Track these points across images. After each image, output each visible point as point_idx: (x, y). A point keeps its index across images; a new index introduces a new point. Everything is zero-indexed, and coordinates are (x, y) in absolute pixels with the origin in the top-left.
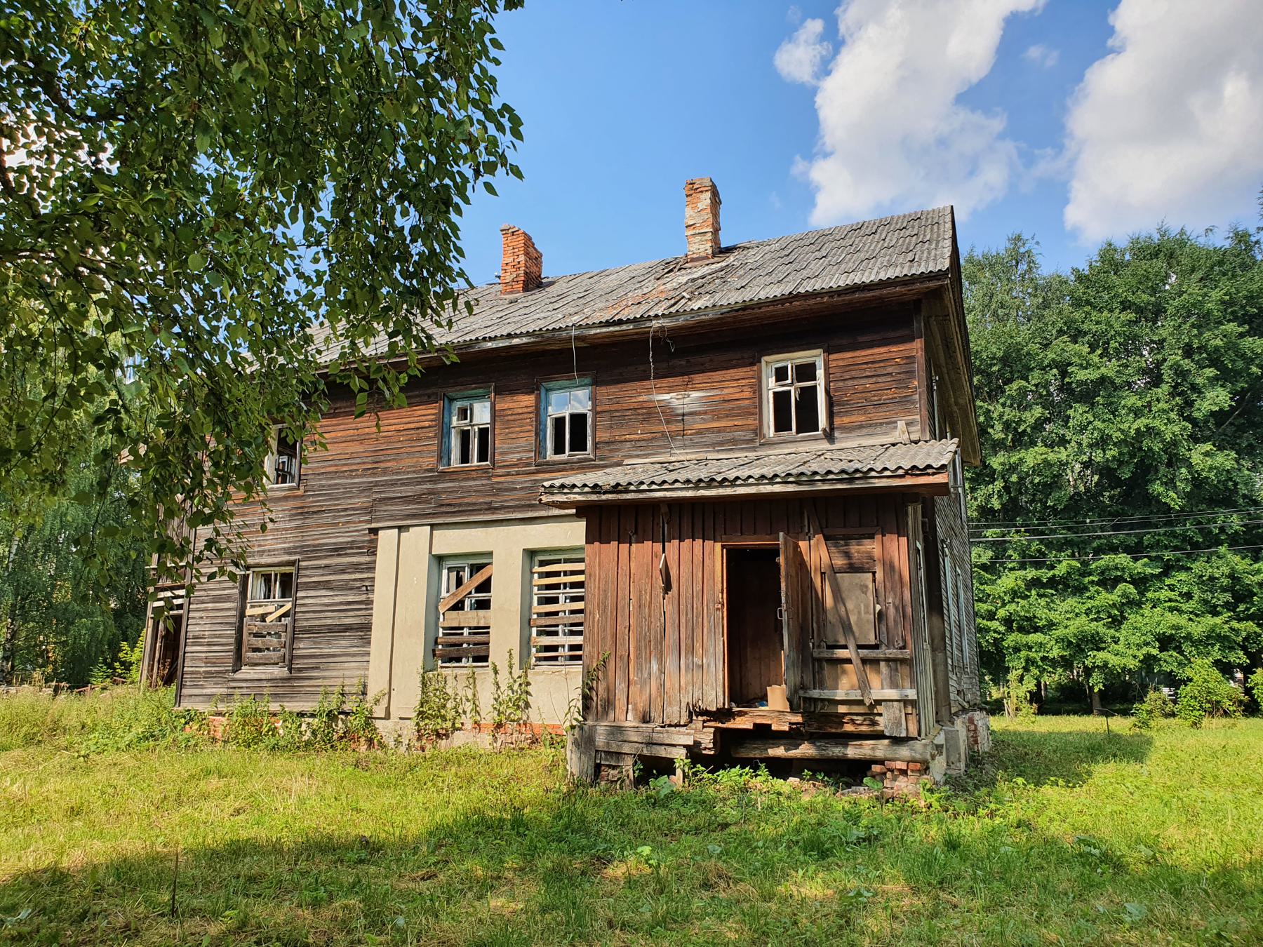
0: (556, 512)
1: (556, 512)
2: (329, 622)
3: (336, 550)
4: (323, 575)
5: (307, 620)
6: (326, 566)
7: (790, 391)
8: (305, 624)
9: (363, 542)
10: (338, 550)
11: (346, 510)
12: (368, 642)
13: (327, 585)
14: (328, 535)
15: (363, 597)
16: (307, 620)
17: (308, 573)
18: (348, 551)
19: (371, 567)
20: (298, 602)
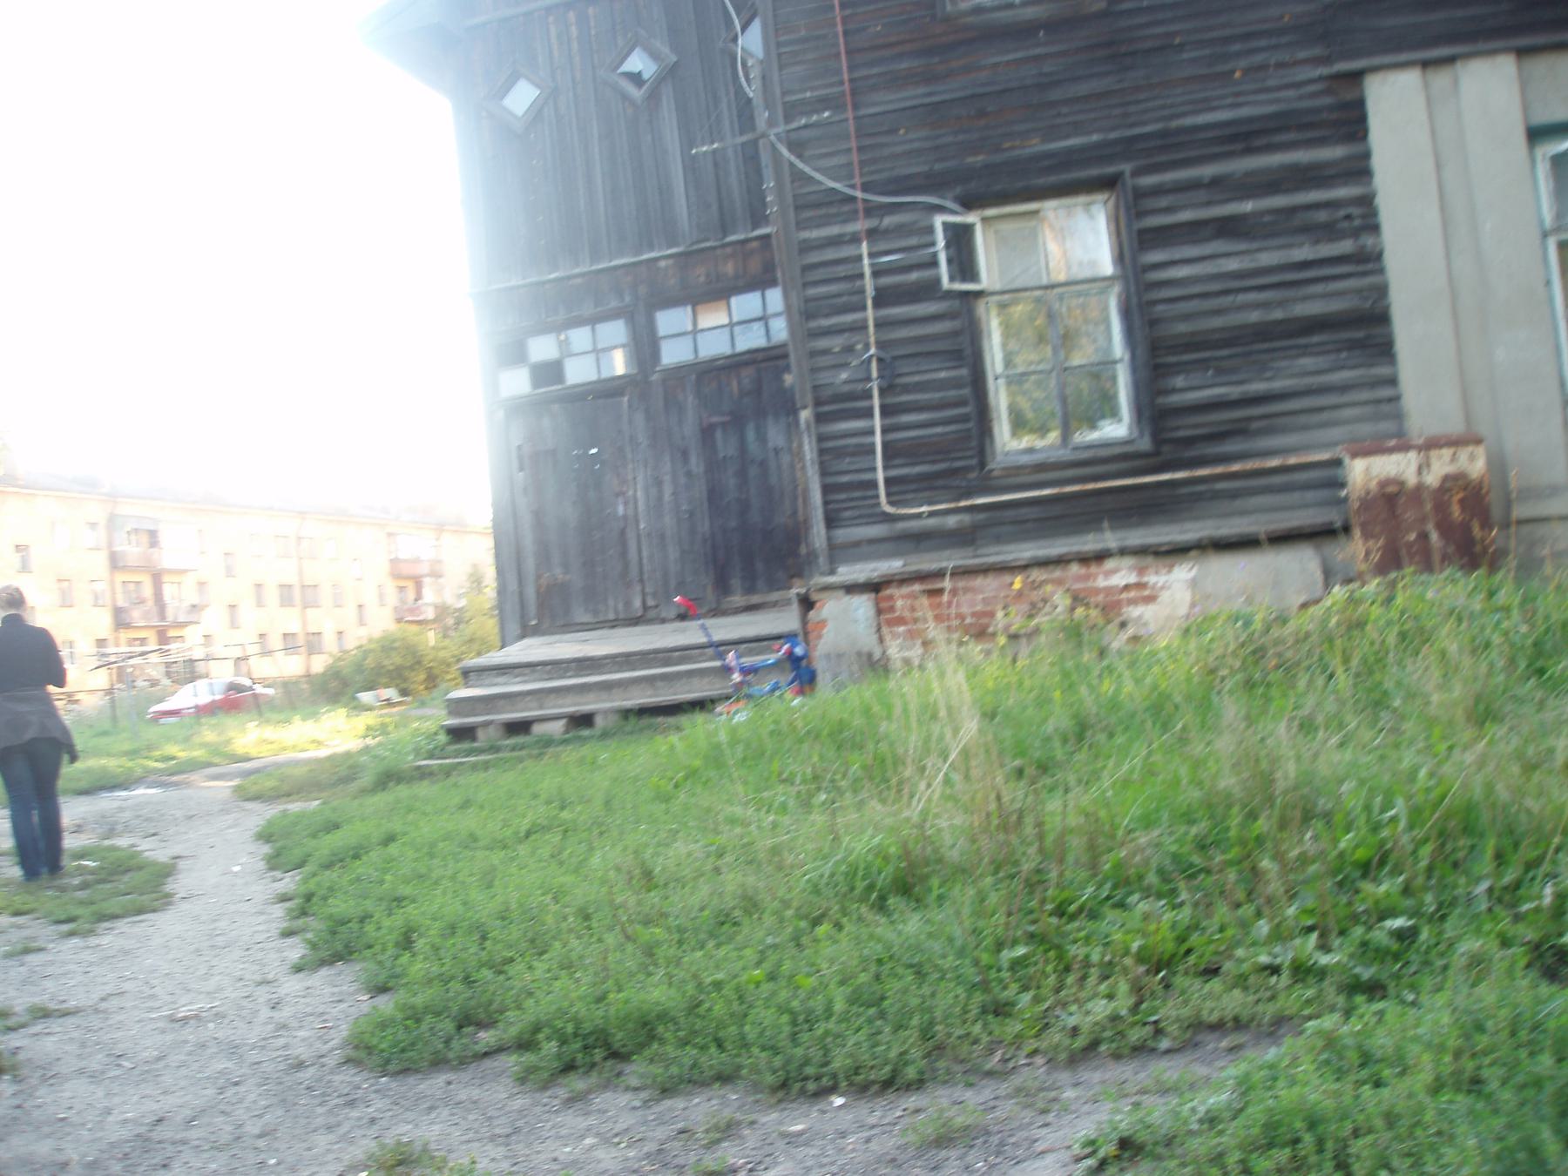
0: (1217, 150)
1: (1217, 150)
2: (1254, 316)
3: (1233, 138)
4: (1209, 204)
5: (1187, 317)
6: (1215, 182)
7: (952, 279)
8: (1182, 328)
9: (1318, 110)
10: (1244, 137)
11: (1247, 36)
12: (1384, 349)
13: (1228, 228)
14: (1206, 105)
15: (1345, 246)
16: (1187, 317)
17: (1163, 202)
18: (1215, 103)
19: (1359, 169)
20: (974, 462)
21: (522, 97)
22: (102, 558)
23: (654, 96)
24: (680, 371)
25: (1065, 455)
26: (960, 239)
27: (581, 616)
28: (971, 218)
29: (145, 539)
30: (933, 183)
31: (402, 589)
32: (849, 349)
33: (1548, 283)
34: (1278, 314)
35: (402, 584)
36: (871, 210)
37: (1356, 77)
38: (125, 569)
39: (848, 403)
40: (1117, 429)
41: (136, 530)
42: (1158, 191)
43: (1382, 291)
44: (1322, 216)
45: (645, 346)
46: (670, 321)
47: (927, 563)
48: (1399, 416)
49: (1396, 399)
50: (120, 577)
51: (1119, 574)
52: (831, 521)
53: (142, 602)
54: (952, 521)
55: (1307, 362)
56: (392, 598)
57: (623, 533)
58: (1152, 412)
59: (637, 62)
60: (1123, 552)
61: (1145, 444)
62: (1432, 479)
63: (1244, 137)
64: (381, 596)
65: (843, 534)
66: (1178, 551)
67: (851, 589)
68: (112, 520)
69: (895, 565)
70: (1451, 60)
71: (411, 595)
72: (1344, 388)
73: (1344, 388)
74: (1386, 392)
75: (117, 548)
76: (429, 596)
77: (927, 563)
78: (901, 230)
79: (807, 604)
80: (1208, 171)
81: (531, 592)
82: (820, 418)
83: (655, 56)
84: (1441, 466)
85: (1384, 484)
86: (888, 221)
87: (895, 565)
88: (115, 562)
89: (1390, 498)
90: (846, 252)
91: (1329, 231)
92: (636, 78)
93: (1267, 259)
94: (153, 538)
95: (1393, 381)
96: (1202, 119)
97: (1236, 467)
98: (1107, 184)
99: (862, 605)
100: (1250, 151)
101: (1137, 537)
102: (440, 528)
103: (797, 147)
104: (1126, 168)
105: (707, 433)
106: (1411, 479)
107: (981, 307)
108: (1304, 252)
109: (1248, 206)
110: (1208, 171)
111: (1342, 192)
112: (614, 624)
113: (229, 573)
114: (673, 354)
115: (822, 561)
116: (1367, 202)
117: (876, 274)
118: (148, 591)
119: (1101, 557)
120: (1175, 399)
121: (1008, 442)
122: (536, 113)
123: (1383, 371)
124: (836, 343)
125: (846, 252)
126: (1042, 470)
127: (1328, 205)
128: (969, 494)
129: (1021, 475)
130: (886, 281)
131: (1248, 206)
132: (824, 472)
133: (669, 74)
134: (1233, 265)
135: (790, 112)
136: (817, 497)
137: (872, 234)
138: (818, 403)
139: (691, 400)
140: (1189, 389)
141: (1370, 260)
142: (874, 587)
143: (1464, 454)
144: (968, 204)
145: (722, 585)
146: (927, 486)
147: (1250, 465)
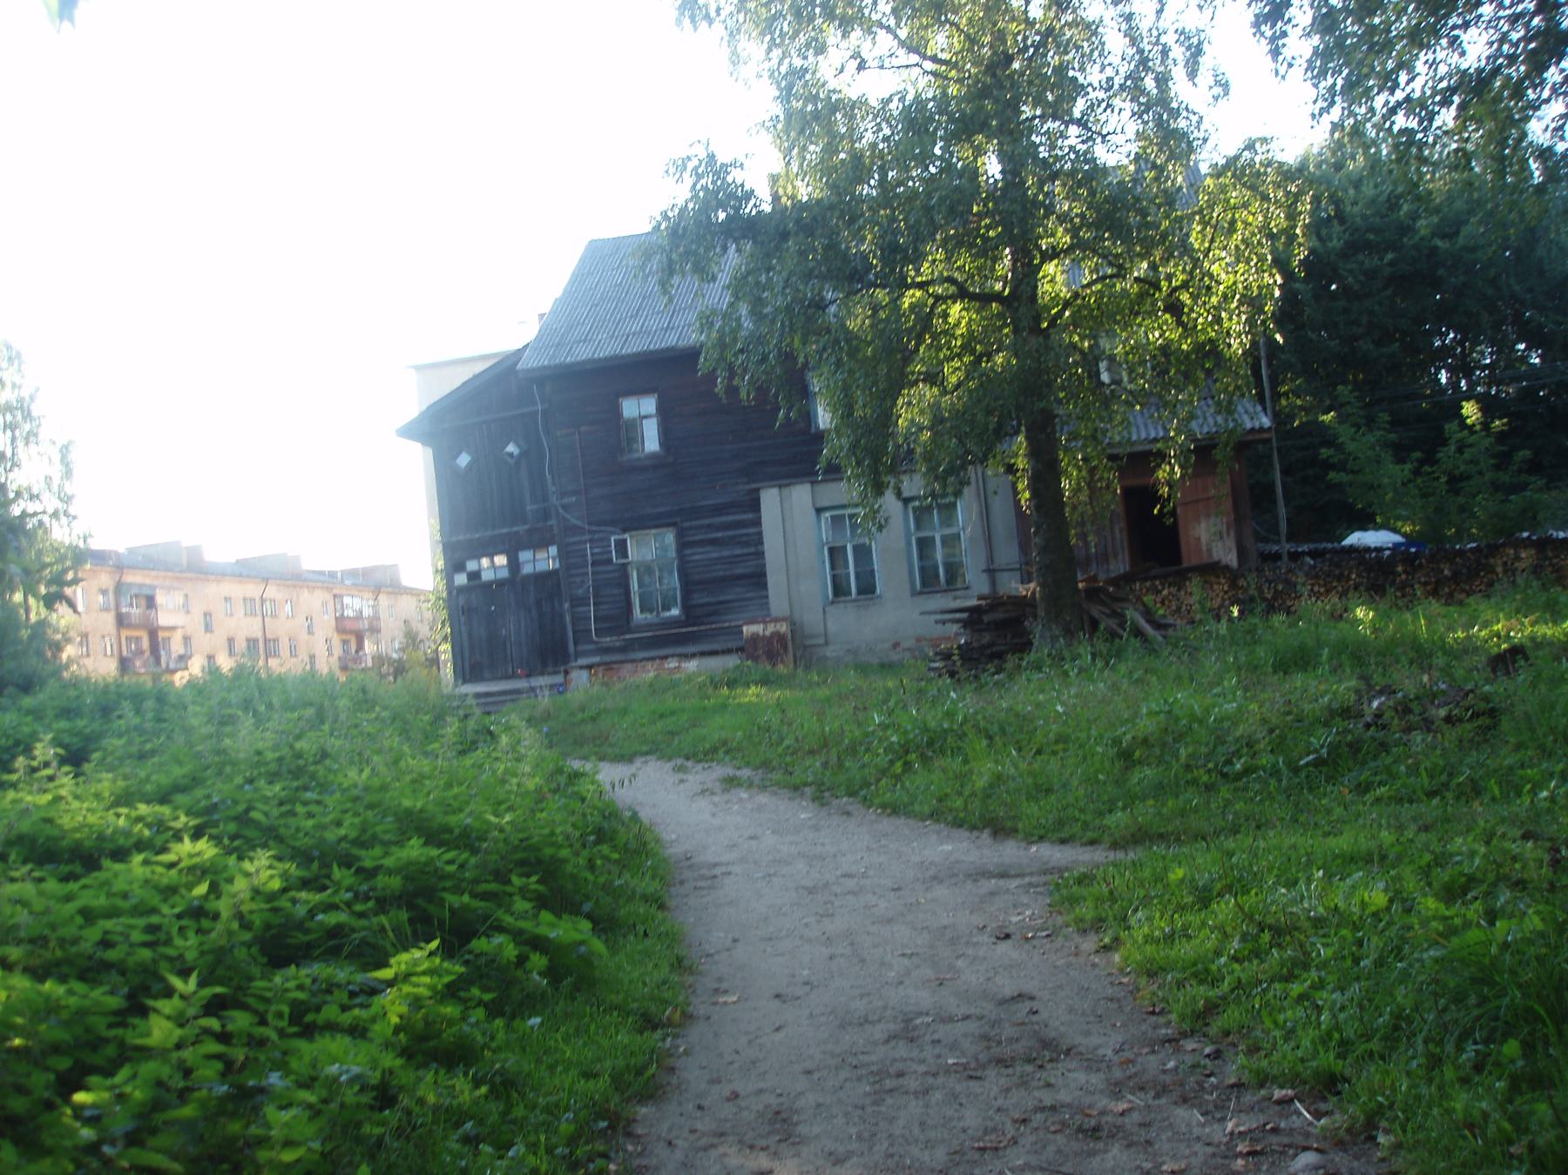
2: (721, 573)
6: (709, 526)
10: (719, 510)
12: (764, 586)
13: (713, 542)
15: (752, 550)
21: (464, 460)
22: (110, 618)
23: (518, 463)
24: (529, 576)
25: (656, 620)
26: (622, 547)
27: (487, 675)
28: (627, 536)
29: (143, 602)
30: (612, 523)
31: (345, 642)
32: (583, 582)
33: (824, 562)
34: (728, 573)
35: (344, 637)
36: (590, 532)
37: (757, 490)
38: (130, 626)
39: (583, 601)
40: (675, 612)
41: (136, 596)
42: (690, 528)
43: (764, 565)
44: (745, 539)
45: (514, 565)
46: (525, 556)
47: (607, 658)
48: (768, 609)
49: (767, 604)
50: (124, 633)
51: (672, 664)
52: (575, 644)
53: (142, 652)
54: (618, 644)
55: (738, 590)
56: (338, 651)
57: (505, 642)
58: (687, 608)
59: (511, 448)
60: (673, 656)
61: (683, 618)
62: (768, 633)
63: (719, 510)
64: (329, 650)
65: (580, 648)
66: (693, 656)
67: (581, 668)
68: (119, 588)
69: (597, 659)
70: (789, 485)
71: (353, 648)
72: (751, 599)
73: (751, 599)
74: (764, 601)
75: (124, 610)
76: (369, 647)
77: (607, 658)
78: (601, 540)
79: (566, 673)
80: (707, 521)
81: (467, 665)
82: (572, 606)
83: (518, 445)
84: (771, 629)
85: (753, 634)
86: (596, 536)
87: (597, 659)
88: (121, 621)
89: (755, 638)
90: (582, 546)
91: (747, 544)
92: (511, 455)
93: (726, 553)
94: (150, 602)
95: (767, 597)
96: (705, 503)
97: (714, 626)
98: (674, 524)
99: (584, 674)
100: (721, 515)
101: (680, 650)
102: (377, 590)
103: (565, 507)
104: (679, 520)
105: (538, 603)
106: (761, 633)
107: (629, 568)
108: (738, 551)
109: (720, 535)
110: (707, 521)
111: (751, 530)
112: (501, 678)
113: (208, 628)
114: (527, 569)
115: (572, 658)
116: (760, 534)
117: (592, 554)
118: (145, 644)
119: (665, 657)
120: (694, 602)
121: (638, 615)
122: (470, 466)
123: (764, 593)
124: (578, 580)
125: (582, 546)
126: (648, 626)
127: (747, 535)
128: (624, 634)
129: (640, 628)
130: (598, 557)
131: (720, 535)
132: (573, 625)
133: (524, 454)
134: (714, 555)
135: (563, 495)
136: (570, 634)
137: (591, 541)
138: (572, 601)
139: (532, 588)
140: (699, 599)
141: (760, 555)
142: (589, 667)
143: (778, 626)
144: (625, 530)
145: (544, 664)
146: (609, 631)
147: (718, 625)
